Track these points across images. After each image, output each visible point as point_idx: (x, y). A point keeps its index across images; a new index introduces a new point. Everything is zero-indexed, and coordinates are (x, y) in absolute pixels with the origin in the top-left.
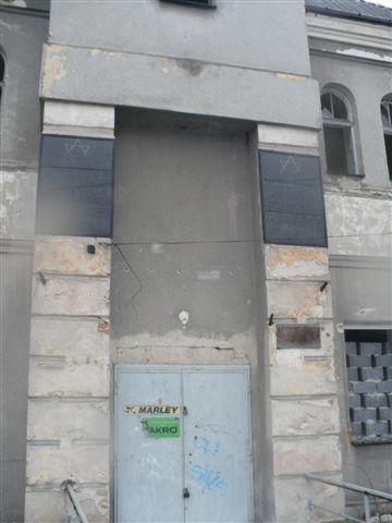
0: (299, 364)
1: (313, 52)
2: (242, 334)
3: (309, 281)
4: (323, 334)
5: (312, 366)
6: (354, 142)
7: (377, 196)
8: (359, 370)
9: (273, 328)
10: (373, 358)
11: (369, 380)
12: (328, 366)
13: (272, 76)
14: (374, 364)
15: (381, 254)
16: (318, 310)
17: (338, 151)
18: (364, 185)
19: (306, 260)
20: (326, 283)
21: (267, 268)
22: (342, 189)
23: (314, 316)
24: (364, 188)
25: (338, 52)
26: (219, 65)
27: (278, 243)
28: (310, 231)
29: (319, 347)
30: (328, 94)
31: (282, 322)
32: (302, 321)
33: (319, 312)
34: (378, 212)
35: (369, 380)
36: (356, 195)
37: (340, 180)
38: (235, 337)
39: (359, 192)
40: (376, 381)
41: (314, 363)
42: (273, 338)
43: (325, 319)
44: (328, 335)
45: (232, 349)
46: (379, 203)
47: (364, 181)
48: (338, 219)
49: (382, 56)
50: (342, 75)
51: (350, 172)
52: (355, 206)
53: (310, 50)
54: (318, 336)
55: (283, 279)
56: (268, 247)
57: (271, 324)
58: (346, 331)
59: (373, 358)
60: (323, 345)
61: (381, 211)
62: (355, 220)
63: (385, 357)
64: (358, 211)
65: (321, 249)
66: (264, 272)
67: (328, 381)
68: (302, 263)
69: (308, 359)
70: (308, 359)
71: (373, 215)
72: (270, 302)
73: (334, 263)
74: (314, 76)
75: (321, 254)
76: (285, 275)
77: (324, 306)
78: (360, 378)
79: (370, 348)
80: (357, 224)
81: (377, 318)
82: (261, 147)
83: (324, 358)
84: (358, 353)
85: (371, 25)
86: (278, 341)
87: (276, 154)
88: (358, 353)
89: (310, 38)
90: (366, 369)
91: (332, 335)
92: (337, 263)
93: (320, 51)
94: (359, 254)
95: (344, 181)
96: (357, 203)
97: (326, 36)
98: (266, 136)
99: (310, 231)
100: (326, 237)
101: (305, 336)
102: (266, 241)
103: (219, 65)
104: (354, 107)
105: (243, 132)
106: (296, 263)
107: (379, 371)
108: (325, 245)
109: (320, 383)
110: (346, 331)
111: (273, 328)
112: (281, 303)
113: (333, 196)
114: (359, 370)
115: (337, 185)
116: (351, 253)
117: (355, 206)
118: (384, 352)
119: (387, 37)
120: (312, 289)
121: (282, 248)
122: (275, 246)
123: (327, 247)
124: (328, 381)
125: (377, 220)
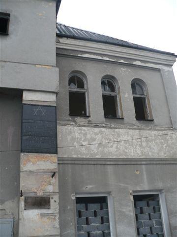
0: (37, 218)
1: (58, 55)
2: (10, 201)
3: (45, 172)
4: (52, 201)
5: (45, 219)
6: (119, 105)
7: (96, 126)
8: (87, 219)
9: (23, 198)
10: (95, 212)
11: (93, 224)
12: (55, 219)
13: (33, 66)
14: (95, 215)
15: (97, 157)
16: (51, 188)
17: (77, 106)
18: (90, 121)
19: (45, 161)
20: (55, 173)
21: (22, 166)
22: (77, 123)
23: (48, 191)
24: (90, 122)
25: (79, 55)
26: (5, 62)
27: (28, 152)
28: (46, 143)
29: (49, 208)
30: (75, 76)
31: (29, 195)
32: (40, 194)
33: (50, 189)
34: (96, 134)
35: (93, 224)
36: (84, 126)
37: (76, 119)
38: (6, 203)
39: (86, 124)
40: (97, 225)
41: (46, 218)
42: (22, 204)
43: (54, 192)
44: (55, 201)
45: (4, 210)
46: (97, 130)
47: (90, 119)
48: (73, 139)
49: (109, 58)
50: (81, 66)
51: (146, 119)
52: (83, 132)
53: (57, 54)
54: (49, 202)
55: (30, 171)
56: (22, 154)
57: (21, 196)
58: (77, 198)
59: (95, 212)
60: (51, 207)
61: (97, 134)
62: (83, 139)
63: (102, 211)
64: (85, 135)
65: (53, 155)
66: (19, 167)
67: (54, 227)
68: (42, 162)
69: (42, 215)
70: (42, 215)
71: (94, 136)
72: (22, 184)
73: (60, 162)
74: (57, 66)
75: (54, 158)
76: (31, 169)
77: (54, 186)
78: (87, 223)
79: (142, 204)
80: (84, 141)
81: (95, 190)
82: (24, 102)
83: (53, 214)
84: (87, 209)
85: (104, 44)
86: (25, 205)
87: (32, 106)
88: (87, 209)
89: (57, 48)
90: (91, 218)
91: (58, 201)
92: (62, 162)
93: (61, 54)
94: (84, 157)
95: (79, 120)
96: (85, 130)
97: (65, 47)
98: (27, 97)
99: (46, 143)
100: (57, 148)
101: (41, 202)
102: (22, 151)
103: (5, 62)
104: (87, 82)
105: (17, 94)
106: (38, 163)
107: (99, 217)
108: (56, 153)
109: (49, 229)
110: (77, 198)
111: (23, 198)
112: (29, 186)
113: (71, 127)
114: (87, 219)
115: (74, 121)
116: (79, 156)
117: (83, 132)
118: (102, 208)
119: (104, 48)
120: (47, 177)
121: (31, 155)
122: (27, 154)
123: (57, 154)
124: (54, 227)
125: (95, 139)
